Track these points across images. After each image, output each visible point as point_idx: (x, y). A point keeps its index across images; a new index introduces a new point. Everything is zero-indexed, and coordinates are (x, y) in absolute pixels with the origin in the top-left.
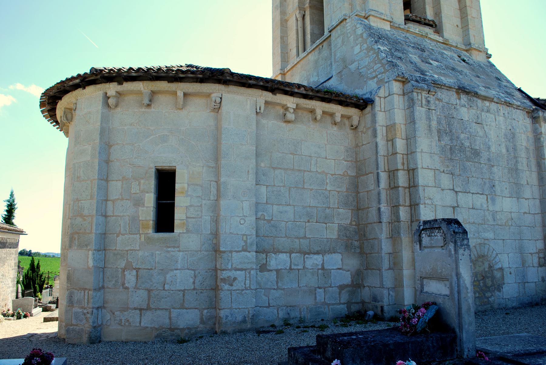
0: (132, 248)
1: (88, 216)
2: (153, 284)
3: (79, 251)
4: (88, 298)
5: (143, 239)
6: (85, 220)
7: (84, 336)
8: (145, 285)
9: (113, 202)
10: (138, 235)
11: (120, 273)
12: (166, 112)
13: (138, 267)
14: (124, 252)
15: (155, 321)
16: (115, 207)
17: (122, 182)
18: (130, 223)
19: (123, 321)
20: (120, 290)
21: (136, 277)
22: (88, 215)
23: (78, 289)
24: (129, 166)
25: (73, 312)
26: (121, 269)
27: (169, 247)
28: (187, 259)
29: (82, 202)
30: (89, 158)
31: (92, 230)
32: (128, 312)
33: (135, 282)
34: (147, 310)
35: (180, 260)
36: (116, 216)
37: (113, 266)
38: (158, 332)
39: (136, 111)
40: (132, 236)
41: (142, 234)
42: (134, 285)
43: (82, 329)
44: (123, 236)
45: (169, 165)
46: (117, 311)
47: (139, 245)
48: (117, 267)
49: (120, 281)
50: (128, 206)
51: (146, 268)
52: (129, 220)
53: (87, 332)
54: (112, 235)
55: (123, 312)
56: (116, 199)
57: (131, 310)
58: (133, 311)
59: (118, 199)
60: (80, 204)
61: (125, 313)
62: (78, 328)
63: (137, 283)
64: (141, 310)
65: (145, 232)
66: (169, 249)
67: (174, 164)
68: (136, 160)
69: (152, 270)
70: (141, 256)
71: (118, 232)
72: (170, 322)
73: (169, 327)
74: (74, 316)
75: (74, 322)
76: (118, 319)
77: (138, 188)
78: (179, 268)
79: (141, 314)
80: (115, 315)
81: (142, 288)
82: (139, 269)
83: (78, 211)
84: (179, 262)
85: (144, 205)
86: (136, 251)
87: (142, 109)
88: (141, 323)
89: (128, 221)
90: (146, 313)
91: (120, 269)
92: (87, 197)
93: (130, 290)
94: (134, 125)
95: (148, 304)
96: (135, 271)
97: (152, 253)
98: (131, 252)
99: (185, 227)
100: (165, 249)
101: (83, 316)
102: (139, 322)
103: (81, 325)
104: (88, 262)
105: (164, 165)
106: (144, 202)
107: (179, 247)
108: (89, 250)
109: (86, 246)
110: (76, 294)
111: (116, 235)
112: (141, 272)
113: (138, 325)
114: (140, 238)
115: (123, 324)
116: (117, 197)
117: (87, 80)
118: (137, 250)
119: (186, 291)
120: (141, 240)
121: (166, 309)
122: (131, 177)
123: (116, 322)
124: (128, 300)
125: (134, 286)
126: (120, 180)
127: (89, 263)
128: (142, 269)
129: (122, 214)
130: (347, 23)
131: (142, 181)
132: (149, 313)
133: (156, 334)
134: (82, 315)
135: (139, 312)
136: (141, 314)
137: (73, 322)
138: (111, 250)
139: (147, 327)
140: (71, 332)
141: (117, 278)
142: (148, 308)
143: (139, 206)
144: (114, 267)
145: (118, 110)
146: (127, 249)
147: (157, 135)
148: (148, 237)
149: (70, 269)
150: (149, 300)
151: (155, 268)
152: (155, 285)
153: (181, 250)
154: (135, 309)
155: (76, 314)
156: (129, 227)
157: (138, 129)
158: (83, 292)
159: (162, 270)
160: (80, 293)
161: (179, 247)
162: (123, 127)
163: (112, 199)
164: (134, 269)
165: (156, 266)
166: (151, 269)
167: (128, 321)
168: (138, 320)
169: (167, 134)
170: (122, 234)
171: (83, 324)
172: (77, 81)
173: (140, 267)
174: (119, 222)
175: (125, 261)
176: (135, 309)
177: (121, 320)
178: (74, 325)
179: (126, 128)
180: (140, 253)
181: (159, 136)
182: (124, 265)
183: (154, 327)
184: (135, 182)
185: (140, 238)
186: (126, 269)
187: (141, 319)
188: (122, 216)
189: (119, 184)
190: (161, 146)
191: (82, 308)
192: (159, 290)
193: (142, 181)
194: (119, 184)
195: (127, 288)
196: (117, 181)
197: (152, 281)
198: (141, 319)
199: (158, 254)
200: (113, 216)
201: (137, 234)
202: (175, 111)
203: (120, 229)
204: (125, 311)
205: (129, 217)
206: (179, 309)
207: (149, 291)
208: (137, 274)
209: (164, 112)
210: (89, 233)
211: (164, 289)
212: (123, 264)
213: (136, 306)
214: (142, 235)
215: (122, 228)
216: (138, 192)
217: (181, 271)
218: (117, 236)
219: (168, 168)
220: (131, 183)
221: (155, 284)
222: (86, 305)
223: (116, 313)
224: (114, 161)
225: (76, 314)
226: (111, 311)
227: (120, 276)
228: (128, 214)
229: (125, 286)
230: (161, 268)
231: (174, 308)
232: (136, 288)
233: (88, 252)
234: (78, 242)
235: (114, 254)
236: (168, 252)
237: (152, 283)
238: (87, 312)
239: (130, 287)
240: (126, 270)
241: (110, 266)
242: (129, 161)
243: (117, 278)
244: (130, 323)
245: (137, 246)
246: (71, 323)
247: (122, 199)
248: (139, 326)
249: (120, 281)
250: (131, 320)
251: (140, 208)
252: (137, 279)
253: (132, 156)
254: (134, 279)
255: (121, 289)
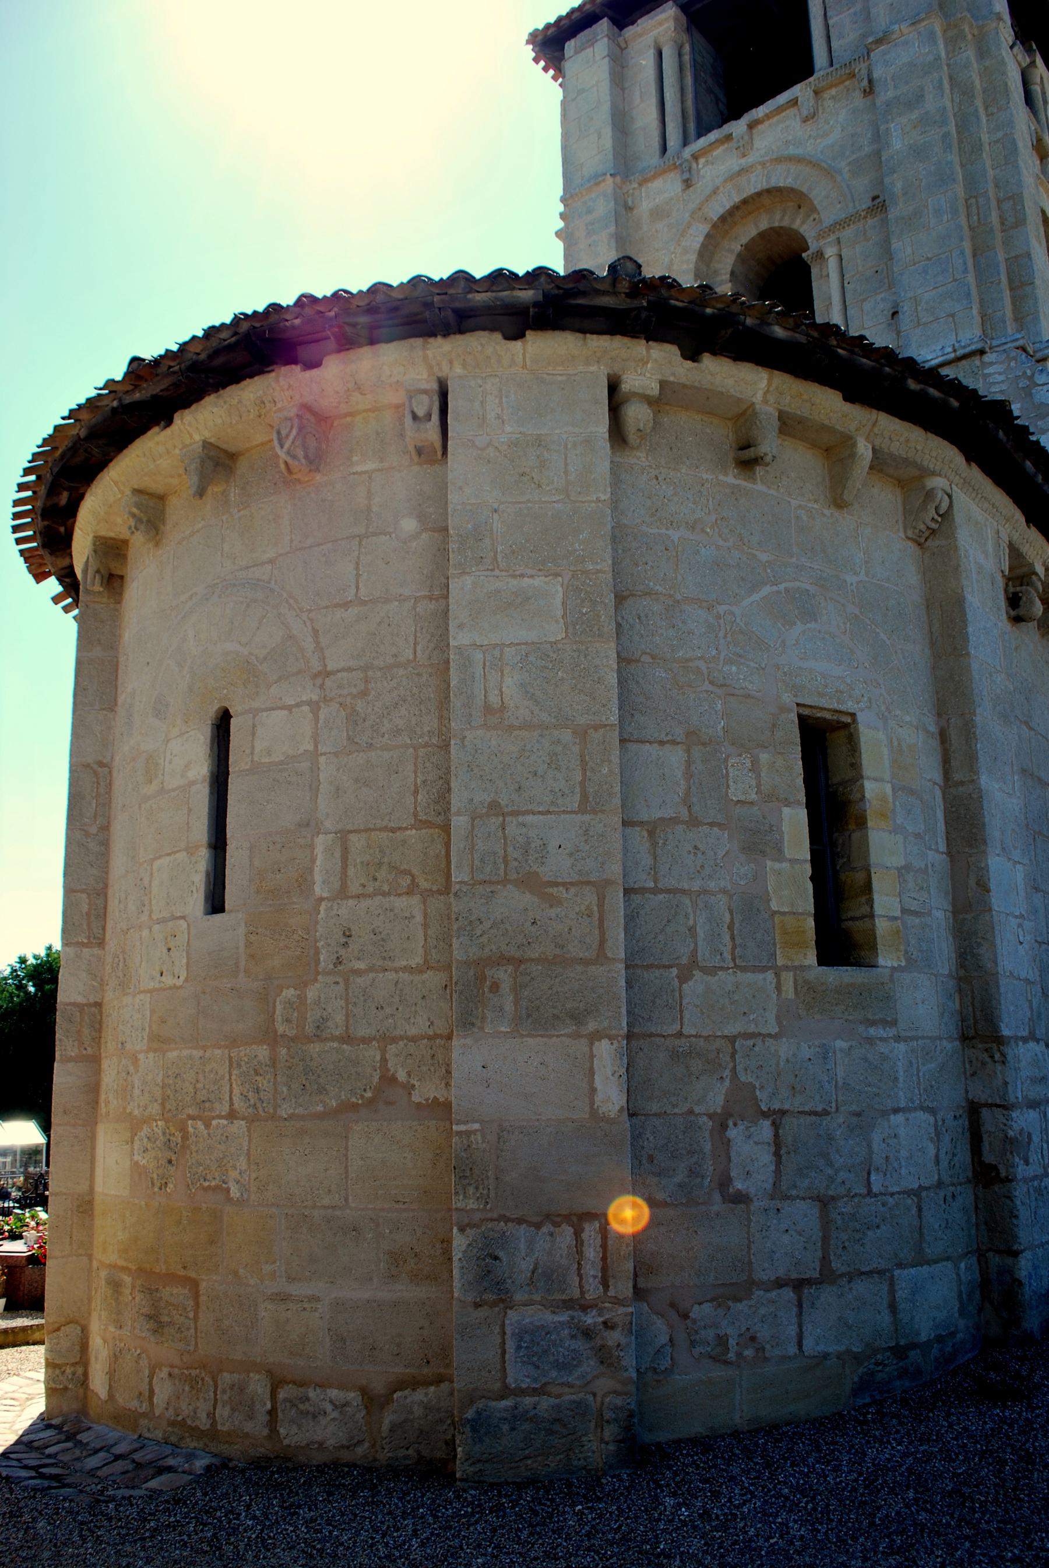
0: (752, 1028)
1: (572, 884)
2: (837, 1171)
3: (530, 1040)
4: (604, 1259)
5: (791, 990)
6: (554, 902)
7: (591, 1436)
8: (807, 1181)
9: (651, 834)
10: (770, 975)
11: (707, 1134)
12: (800, 506)
13: (776, 1106)
14: (719, 1043)
15: (849, 1327)
16: (659, 851)
17: (688, 751)
18: (737, 925)
19: (732, 1342)
20: (715, 1208)
21: (773, 1149)
22: (576, 878)
23: (538, 1219)
24: (711, 688)
25: (508, 1330)
26: (710, 1116)
27: (872, 1023)
28: (918, 1071)
29: (529, 819)
30: (555, 631)
31: (608, 944)
32: (752, 1303)
33: (773, 1168)
34: (821, 1283)
35: (902, 1073)
36: (668, 891)
37: (674, 1106)
38: (861, 1370)
39: (705, 476)
40: (750, 977)
41: (787, 968)
42: (771, 1181)
43: (578, 1404)
44: (708, 978)
45: (835, 706)
46: (700, 1304)
47: (778, 1017)
48: (691, 1112)
49: (709, 1168)
50: (721, 853)
51: (807, 1109)
52: (731, 912)
53: (608, 1415)
54: (657, 973)
55: (730, 1303)
56: (662, 819)
57: (762, 1293)
58: (773, 1294)
59: (675, 821)
60: (512, 829)
61: (740, 1306)
62: (545, 1403)
63: (778, 1172)
64: (799, 1285)
65: (796, 963)
66: (872, 1031)
67: (849, 706)
68: (734, 668)
69: (829, 1118)
70: (788, 1061)
71: (684, 961)
72: (896, 1322)
73: (892, 1344)
74: (519, 1348)
75: (517, 1375)
76: (710, 1334)
77: (754, 783)
78: (902, 1105)
79: (800, 1305)
80: (694, 1321)
81: (802, 1194)
82: (783, 1113)
83: (506, 862)
84: (901, 1080)
85: (780, 851)
86: (769, 1042)
87: (726, 474)
88: (805, 1342)
89: (727, 916)
90: (818, 1298)
91: (705, 1119)
92: (560, 802)
93: (755, 1205)
94: (703, 530)
95: (825, 1259)
96: (766, 1124)
97: (824, 1045)
98: (750, 1043)
99: (902, 947)
100: (861, 1028)
101: (579, 1344)
102: (795, 1340)
103: (571, 1386)
104: (593, 1090)
105: (823, 702)
106: (782, 841)
107: (894, 1023)
108: (595, 1037)
109: (577, 1018)
110: (522, 1246)
111: (674, 971)
112: (791, 1126)
113: (792, 1350)
114: (778, 987)
115: (731, 1356)
116: (668, 813)
117: (581, 301)
118: (770, 1035)
119: (924, 1194)
120: (783, 995)
121: (881, 1272)
122: (721, 734)
123: (697, 1351)
124: (749, 1247)
125: (769, 1186)
126: (675, 743)
127: (598, 1098)
128: (793, 1112)
129: (696, 886)
130: (984, 365)
131: (764, 757)
132: (827, 1295)
133: (856, 1379)
134: (573, 1337)
135: (791, 1294)
136: (800, 1305)
137: (510, 1380)
138: (658, 1035)
139: (826, 1356)
140: (505, 1427)
141: (694, 1159)
142: (827, 1276)
143: (763, 853)
144: (676, 1110)
145: (639, 458)
146: (730, 1030)
147: (782, 587)
148: (806, 982)
149: (476, 1126)
150: (825, 1239)
151: (837, 1109)
152: (842, 1175)
153: (903, 1034)
154: (780, 1284)
155: (527, 1338)
156: (733, 938)
157: (718, 548)
158: (568, 1231)
159: (858, 1114)
160: (551, 1235)
161: (894, 1023)
162: (664, 531)
163: (644, 816)
164: (765, 1115)
165: (840, 1098)
166: (826, 1113)
167: (753, 1339)
168: (792, 1331)
169: (808, 587)
170: (706, 971)
171: (578, 1383)
172: (527, 295)
173: (786, 1107)
174: (687, 916)
175: (727, 1083)
176: (780, 1284)
177: (722, 1341)
178: (521, 1392)
179: (675, 535)
180: (784, 1049)
181: (787, 590)
182: (720, 1100)
183: (848, 1352)
184: (740, 755)
185: (778, 987)
186: (731, 1115)
187: (800, 1326)
188: (699, 894)
189: (675, 758)
190: (804, 632)
191: (568, 1304)
192: (856, 1195)
193: (764, 757)
194: (675, 758)
195: (741, 1199)
196: (662, 743)
197: (830, 1164)
198: (800, 1326)
199: (841, 1050)
200: (655, 891)
201: (763, 969)
202: (827, 512)
203: (695, 950)
204: (740, 1300)
205: (731, 897)
206: (913, 1266)
207: (825, 1203)
208: (776, 1135)
209: (794, 503)
210: (586, 962)
211: (870, 1193)
212: (716, 1098)
213: (781, 1272)
214: (784, 974)
215: (700, 943)
216: (753, 796)
217: (907, 1115)
218: (683, 978)
219: (828, 716)
220: (726, 760)
221: (842, 1173)
222: (593, 1290)
223: (696, 1312)
224: (638, 661)
225: (527, 1338)
226: (673, 1305)
227: (708, 1147)
228: (723, 884)
229: (731, 1190)
230: (854, 1107)
231: (900, 1265)
232: (778, 1193)
233: (592, 1044)
234: (516, 1002)
235: (676, 1055)
236: (870, 1041)
237: (830, 1172)
238: (605, 1323)
239: (752, 1191)
240: (731, 1123)
241: (655, 1107)
242: (705, 672)
243: (694, 1159)
244: (763, 1349)
245: (771, 1016)
246: (498, 1385)
247: (693, 822)
248: (795, 1356)
249: (709, 1168)
250: (764, 1334)
251: (769, 863)
252: (777, 1154)
253: (714, 652)
254: (765, 1158)
255: (717, 1205)
